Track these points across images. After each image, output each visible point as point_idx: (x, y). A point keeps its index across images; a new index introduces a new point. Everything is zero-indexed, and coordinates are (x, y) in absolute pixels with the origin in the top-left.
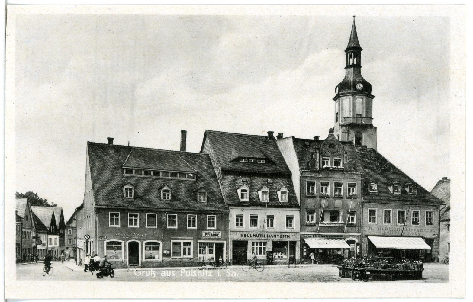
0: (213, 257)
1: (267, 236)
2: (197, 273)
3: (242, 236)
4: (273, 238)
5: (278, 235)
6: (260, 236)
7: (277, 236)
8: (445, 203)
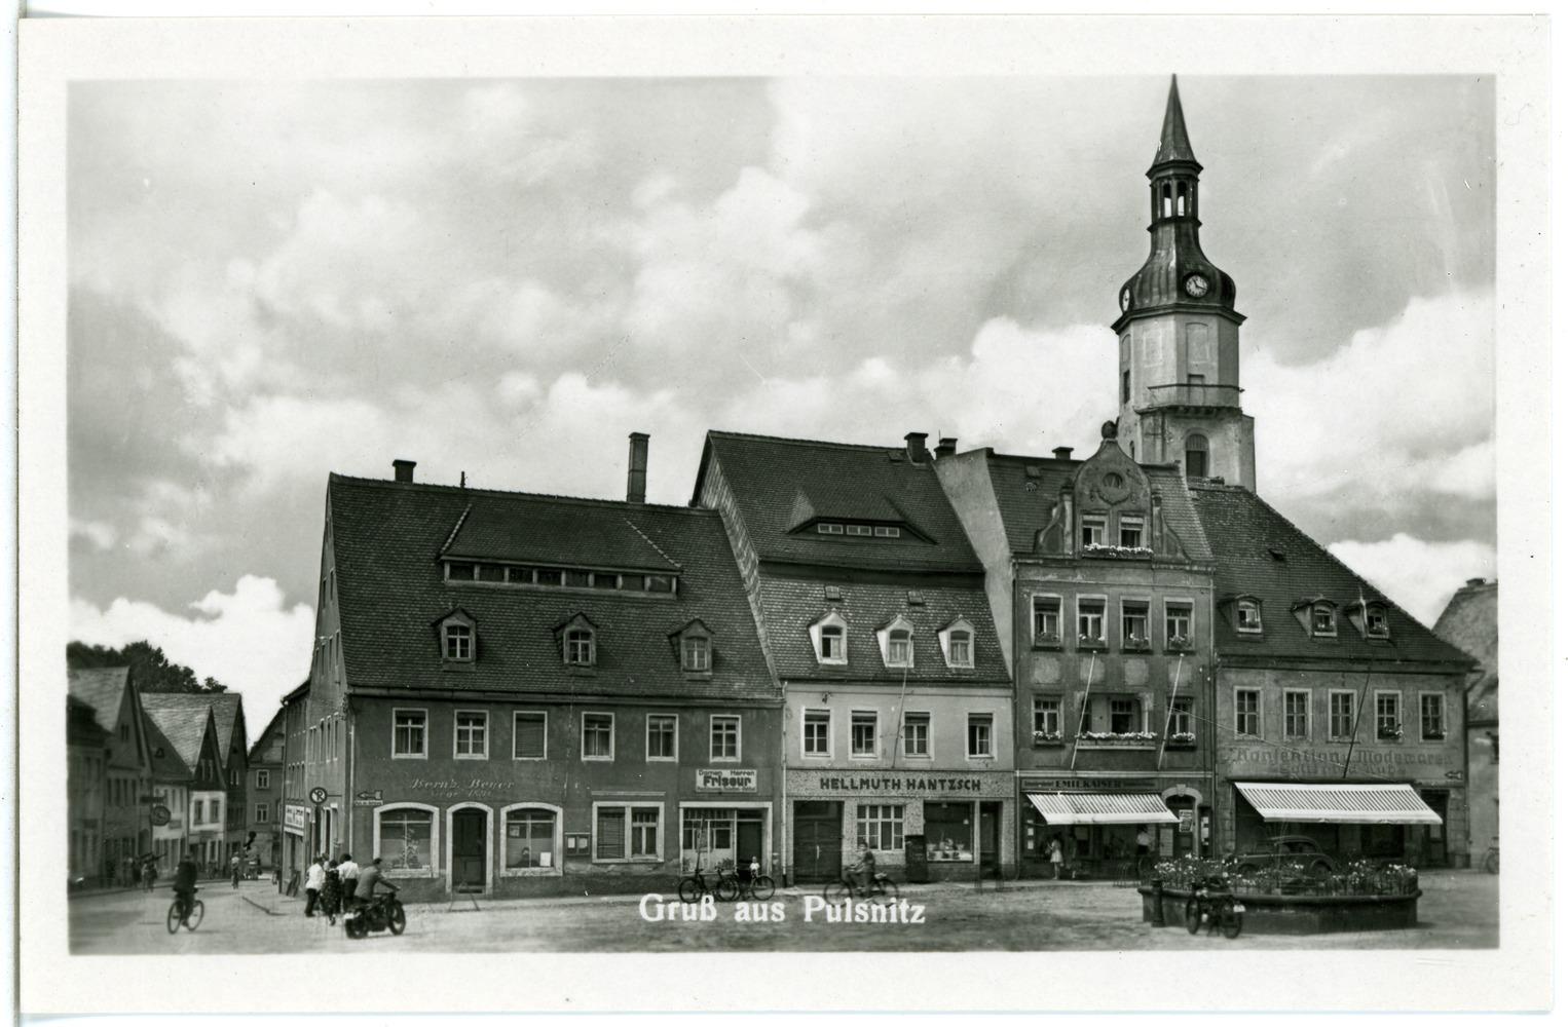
1: (905, 784)
3: (824, 784)
4: (927, 791)
5: (942, 781)
6: (882, 784)
7: (939, 785)
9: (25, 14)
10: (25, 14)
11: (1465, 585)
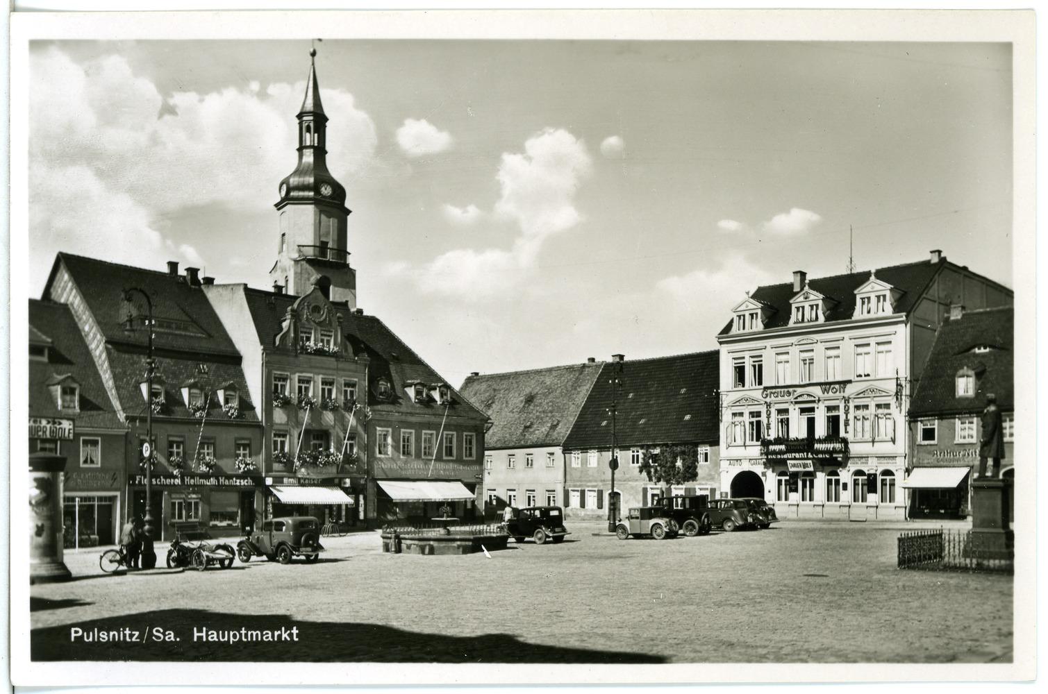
0: (844, 491)
2: (108, 636)
8: (491, 419)
9: (14, 9)
10: (14, 9)
11: (470, 375)
